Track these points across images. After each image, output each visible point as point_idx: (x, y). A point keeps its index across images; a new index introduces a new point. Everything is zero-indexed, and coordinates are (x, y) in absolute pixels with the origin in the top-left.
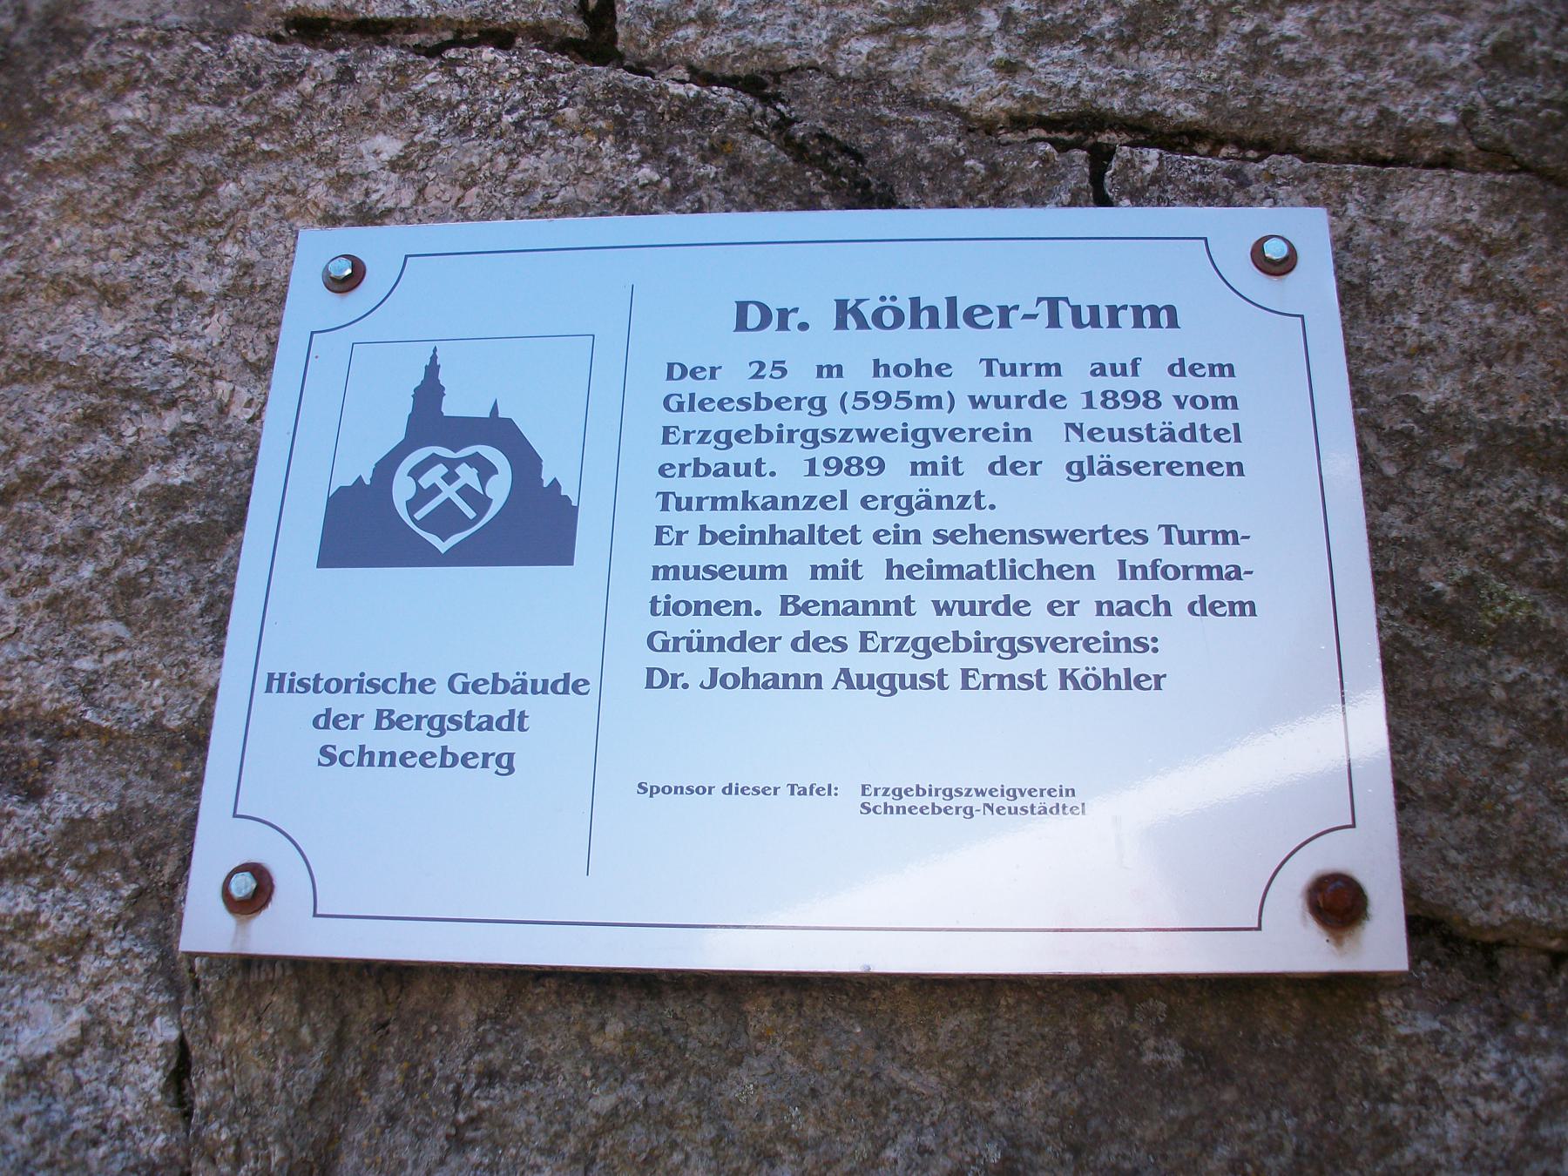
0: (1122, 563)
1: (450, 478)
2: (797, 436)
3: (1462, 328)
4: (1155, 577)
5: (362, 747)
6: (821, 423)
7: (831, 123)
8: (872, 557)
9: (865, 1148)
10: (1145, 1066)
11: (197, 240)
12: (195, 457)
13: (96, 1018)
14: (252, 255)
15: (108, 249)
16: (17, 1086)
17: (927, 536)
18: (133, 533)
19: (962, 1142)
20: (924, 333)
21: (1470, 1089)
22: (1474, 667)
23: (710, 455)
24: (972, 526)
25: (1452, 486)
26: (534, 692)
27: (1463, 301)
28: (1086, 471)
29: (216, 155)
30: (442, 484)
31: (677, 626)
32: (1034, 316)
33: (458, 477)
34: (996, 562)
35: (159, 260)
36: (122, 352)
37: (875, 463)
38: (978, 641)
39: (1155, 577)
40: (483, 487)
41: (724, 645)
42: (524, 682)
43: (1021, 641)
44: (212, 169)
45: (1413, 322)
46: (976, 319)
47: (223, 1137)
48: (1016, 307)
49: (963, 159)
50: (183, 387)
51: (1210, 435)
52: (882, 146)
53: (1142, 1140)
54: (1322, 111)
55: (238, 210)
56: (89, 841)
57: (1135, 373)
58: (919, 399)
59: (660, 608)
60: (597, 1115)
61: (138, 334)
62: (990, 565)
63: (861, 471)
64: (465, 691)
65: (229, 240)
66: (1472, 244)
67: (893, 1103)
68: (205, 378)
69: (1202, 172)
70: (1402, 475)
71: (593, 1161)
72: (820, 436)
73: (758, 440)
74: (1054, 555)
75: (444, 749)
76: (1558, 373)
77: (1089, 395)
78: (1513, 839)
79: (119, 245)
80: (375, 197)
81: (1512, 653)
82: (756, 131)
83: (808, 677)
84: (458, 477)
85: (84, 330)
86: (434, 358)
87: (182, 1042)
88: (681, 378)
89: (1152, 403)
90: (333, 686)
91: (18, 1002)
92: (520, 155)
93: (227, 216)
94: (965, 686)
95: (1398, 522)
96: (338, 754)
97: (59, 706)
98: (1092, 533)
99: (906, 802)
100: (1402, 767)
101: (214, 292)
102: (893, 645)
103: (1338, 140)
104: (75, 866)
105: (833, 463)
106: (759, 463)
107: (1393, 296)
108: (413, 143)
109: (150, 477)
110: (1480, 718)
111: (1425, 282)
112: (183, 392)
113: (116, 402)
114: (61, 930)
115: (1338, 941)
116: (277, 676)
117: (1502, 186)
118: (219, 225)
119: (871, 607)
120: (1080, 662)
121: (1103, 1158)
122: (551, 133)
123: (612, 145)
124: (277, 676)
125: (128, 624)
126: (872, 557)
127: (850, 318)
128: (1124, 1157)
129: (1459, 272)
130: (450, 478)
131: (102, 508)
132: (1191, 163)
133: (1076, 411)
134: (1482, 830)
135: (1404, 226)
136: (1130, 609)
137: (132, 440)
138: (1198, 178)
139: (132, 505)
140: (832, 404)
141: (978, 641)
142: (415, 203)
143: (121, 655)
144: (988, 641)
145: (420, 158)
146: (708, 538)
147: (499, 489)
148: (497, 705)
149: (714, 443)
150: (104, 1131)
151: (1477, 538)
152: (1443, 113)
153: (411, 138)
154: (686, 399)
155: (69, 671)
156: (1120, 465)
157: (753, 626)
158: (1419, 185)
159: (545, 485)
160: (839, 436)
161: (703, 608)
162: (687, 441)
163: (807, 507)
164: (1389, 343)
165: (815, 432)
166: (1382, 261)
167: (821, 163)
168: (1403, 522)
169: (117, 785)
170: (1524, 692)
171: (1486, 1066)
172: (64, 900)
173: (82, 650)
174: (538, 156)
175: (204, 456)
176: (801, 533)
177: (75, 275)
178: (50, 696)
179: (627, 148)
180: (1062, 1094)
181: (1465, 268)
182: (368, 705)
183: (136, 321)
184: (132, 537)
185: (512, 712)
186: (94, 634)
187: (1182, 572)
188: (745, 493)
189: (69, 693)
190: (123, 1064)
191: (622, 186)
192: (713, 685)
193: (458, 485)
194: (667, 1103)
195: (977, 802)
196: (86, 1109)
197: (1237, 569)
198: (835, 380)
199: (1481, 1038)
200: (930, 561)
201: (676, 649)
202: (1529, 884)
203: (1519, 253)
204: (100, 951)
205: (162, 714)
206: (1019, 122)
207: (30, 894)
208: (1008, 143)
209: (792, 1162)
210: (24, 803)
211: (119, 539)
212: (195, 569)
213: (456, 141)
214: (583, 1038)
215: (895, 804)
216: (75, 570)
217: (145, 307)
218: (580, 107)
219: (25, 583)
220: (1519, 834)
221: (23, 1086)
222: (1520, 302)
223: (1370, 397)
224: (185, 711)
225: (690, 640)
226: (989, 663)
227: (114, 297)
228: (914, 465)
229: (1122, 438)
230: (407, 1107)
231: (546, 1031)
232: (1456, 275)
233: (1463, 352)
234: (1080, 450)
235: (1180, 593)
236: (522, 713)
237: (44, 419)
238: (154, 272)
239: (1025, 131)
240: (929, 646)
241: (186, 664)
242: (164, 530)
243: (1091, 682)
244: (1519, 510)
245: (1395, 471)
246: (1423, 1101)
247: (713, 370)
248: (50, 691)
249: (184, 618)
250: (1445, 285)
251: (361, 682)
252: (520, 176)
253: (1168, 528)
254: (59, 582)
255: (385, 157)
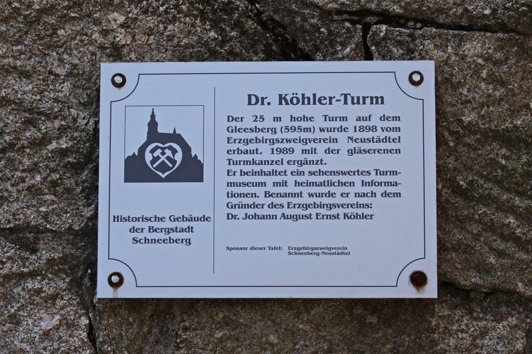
0: (363, 181)
1: (163, 154)
2: (268, 141)
3: (481, 94)
4: (372, 185)
5: (145, 238)
6: (275, 137)
7: (275, 13)
8: (290, 179)
9: (291, 346)
10: (367, 323)
11: (52, 52)
12: (68, 138)
13: (64, 318)
14: (76, 61)
15: (20, 55)
16: (42, 338)
17: (306, 173)
18: (52, 165)
19: (317, 344)
20: (306, 106)
21: (458, 330)
22: (470, 208)
23: (242, 147)
24: (320, 170)
25: (471, 150)
26: (195, 221)
27: (483, 84)
28: (353, 152)
29: (54, 17)
30: (161, 156)
31: (235, 201)
32: (339, 100)
33: (165, 153)
34: (326, 181)
35: (41, 60)
36: (34, 97)
37: (291, 150)
38: (321, 205)
39: (372, 185)
40: (174, 156)
41: (249, 206)
42: (192, 218)
43: (333, 205)
44: (54, 24)
45: (465, 92)
46: (322, 101)
47: (109, 350)
48: (334, 97)
49: (320, 28)
50: (59, 111)
51: (391, 140)
52: (293, 23)
53: (366, 343)
54: (444, 9)
55: (67, 42)
56: (54, 266)
57: (370, 120)
58: (304, 129)
59: (230, 195)
60: (217, 339)
61: (38, 90)
62: (324, 182)
63: (287, 152)
64: (174, 221)
65: (65, 53)
66: (490, 61)
67: (298, 333)
68: (66, 108)
69: (400, 36)
70: (455, 146)
71: (216, 351)
72: (275, 141)
73: (256, 142)
74: (343, 179)
75: (170, 238)
76: (512, 109)
77: (355, 127)
78: (476, 260)
79: (24, 54)
80: (118, 39)
81: (482, 204)
82: (249, 17)
83: (273, 216)
84: (165, 153)
85: (17, 88)
86: (153, 112)
87: (90, 323)
88: (232, 121)
89: (374, 130)
90: (134, 219)
91: (38, 315)
92: (168, 24)
93: (63, 44)
94: (317, 218)
95: (452, 162)
96: (138, 240)
97: (37, 223)
98: (354, 172)
99: (301, 251)
100: (445, 239)
101: (63, 74)
102: (297, 206)
103: (448, 20)
104: (51, 273)
105: (279, 150)
106: (257, 150)
107: (460, 82)
108: (128, 18)
109: (53, 146)
110: (470, 224)
111: (471, 77)
112: (59, 113)
113: (36, 116)
114: (50, 293)
115: (418, 290)
116: (116, 217)
117: (502, 39)
118: (61, 47)
119: (290, 195)
120: (349, 211)
121: (355, 348)
122: (178, 16)
123: (200, 22)
124: (116, 217)
125: (55, 195)
126: (290, 179)
127: (283, 100)
128: (361, 348)
129: (483, 73)
130: (163, 154)
131: (37, 155)
132: (397, 31)
133: (351, 133)
134: (466, 258)
135: (466, 56)
136: (365, 195)
137: (45, 131)
138: (398, 38)
139: (50, 155)
140: (278, 130)
141: (321, 205)
142: (132, 42)
143: (54, 206)
144: (324, 205)
145: (131, 23)
146: (243, 174)
147: (179, 157)
148: (185, 225)
149: (243, 143)
150: (70, 350)
151: (477, 167)
152: (486, 9)
153: (128, 15)
154: (234, 128)
155: (38, 211)
156: (363, 150)
157: (257, 201)
158: (474, 39)
159: (193, 156)
160: (280, 141)
161: (242, 195)
162: (235, 142)
163: (271, 164)
164: (457, 99)
165: (273, 139)
166: (457, 70)
167: (272, 31)
168: (454, 161)
169: (60, 248)
170: (484, 217)
171: (463, 324)
172: (49, 284)
173: (41, 205)
174: (174, 24)
175: (71, 137)
176: (270, 172)
177: (9, 65)
178: (34, 220)
179: (205, 23)
180: (344, 331)
181: (485, 71)
182: (146, 225)
183: (37, 85)
184: (52, 166)
185: (189, 227)
186: (45, 199)
187: (380, 184)
188: (253, 159)
189: (40, 219)
190: (73, 331)
191: (205, 40)
192: (246, 218)
193: (166, 156)
194: (236, 335)
195: (320, 251)
196: (64, 344)
197: (396, 183)
198: (279, 123)
199: (463, 317)
200: (307, 181)
201: (235, 208)
202: (480, 273)
203: (505, 65)
204: (62, 299)
205: (72, 225)
206: (339, 12)
207: (39, 282)
208: (336, 21)
209: (271, 350)
210: (31, 254)
211: (47, 166)
212: (75, 176)
213: (143, 16)
214: (211, 317)
215: (297, 252)
216: (33, 177)
217: (39, 79)
218: (187, 5)
219: (17, 182)
220: (477, 259)
221: (44, 338)
222: (503, 84)
223: (448, 119)
224: (80, 224)
225: (239, 205)
226: (324, 211)
227: (25, 74)
228: (303, 150)
229: (364, 142)
230: (161, 339)
231: (201, 316)
232: (482, 74)
233: (480, 103)
234: (352, 145)
235: (379, 190)
236: (192, 227)
237: (9, 121)
238: (39, 65)
239: (342, 15)
240: (307, 207)
241: (78, 209)
242: (62, 164)
243: (352, 217)
244: (490, 158)
245: (453, 144)
246: (444, 333)
247: (242, 118)
248: (34, 219)
249: (75, 194)
250: (477, 78)
251: (143, 218)
252: (168, 33)
253: (377, 170)
254: (29, 182)
255: (118, 22)
